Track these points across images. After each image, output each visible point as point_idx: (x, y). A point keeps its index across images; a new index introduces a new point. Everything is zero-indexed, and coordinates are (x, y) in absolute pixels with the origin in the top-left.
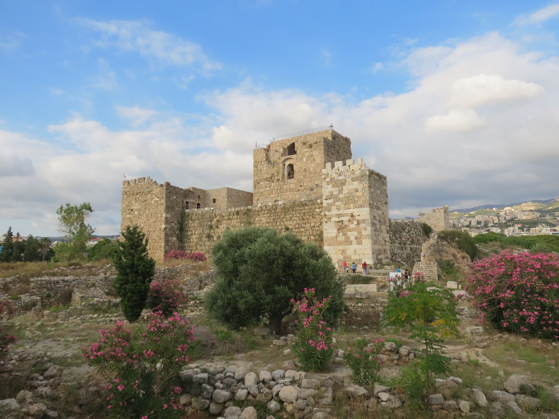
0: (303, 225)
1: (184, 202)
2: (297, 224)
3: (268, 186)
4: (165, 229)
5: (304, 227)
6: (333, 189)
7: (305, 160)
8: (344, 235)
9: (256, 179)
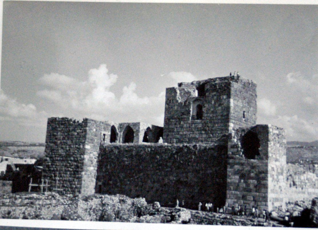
1: (102, 134)
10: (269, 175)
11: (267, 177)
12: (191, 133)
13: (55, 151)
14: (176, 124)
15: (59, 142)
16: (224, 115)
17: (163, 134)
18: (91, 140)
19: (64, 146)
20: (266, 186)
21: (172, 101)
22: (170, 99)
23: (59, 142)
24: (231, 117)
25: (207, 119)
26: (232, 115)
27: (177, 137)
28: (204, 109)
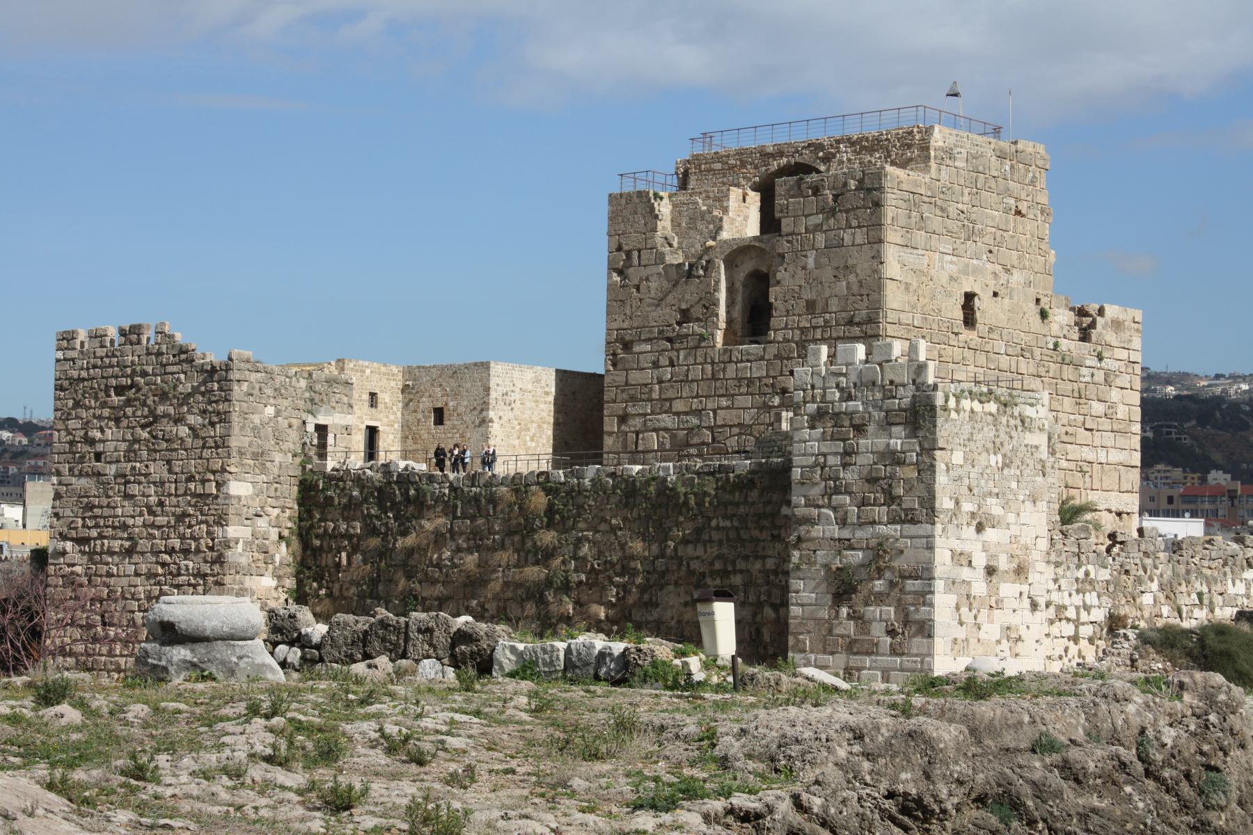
0: (741, 565)
1: (310, 428)
2: (718, 557)
3: (664, 361)
4: (221, 520)
5: (741, 572)
6: (827, 447)
7: (811, 262)
8: (854, 616)
9: (615, 325)
10: (939, 585)
11: (932, 593)
12: (724, 402)
13: (97, 511)
14: (656, 365)
15: (111, 470)
16: (857, 320)
17: (605, 412)
18: (255, 456)
19: (134, 489)
20: (925, 629)
21: (635, 254)
22: (626, 248)
23: (111, 470)
24: (891, 330)
25: (788, 341)
26: (892, 317)
27: (663, 425)
28: (774, 294)
